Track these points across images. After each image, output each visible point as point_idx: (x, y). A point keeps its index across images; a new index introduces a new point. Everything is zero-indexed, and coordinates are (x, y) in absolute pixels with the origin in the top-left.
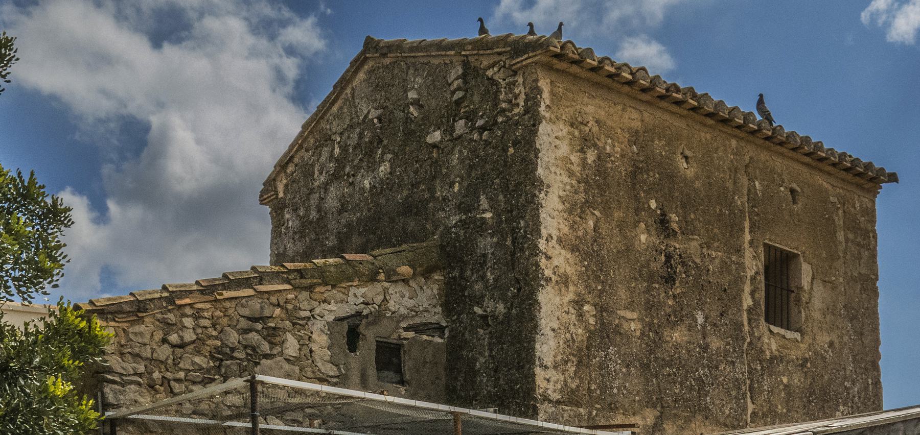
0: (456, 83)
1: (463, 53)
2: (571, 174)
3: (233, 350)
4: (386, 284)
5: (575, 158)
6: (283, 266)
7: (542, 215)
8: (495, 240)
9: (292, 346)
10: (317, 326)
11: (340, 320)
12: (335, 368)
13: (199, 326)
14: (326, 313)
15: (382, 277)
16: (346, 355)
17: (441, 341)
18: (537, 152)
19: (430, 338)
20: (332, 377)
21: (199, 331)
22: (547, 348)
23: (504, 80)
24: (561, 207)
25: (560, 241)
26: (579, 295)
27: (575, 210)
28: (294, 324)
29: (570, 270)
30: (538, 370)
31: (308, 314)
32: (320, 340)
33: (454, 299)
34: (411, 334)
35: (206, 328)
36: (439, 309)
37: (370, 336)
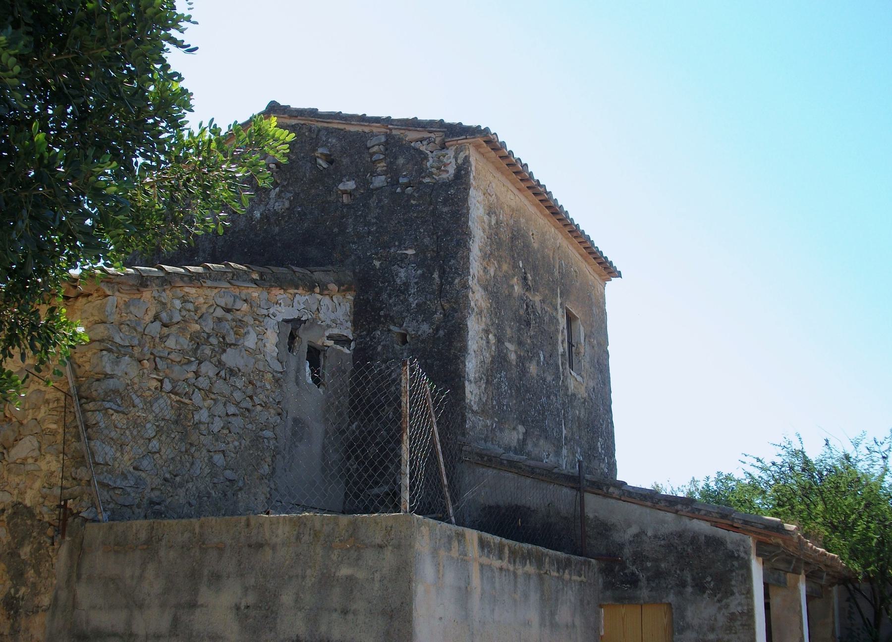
2: (484, 231)
4: (319, 297)
5: (486, 218)
7: (471, 258)
8: (419, 272)
10: (271, 322)
11: (287, 321)
12: (280, 365)
14: (278, 313)
15: (317, 290)
17: (348, 351)
19: (341, 348)
20: (276, 372)
21: (184, 313)
23: (432, 152)
25: (478, 281)
26: (487, 325)
27: (486, 257)
29: (483, 305)
30: (467, 383)
31: (265, 312)
32: (272, 338)
33: (366, 314)
34: (331, 343)
35: (189, 311)
36: (349, 324)
37: (306, 338)
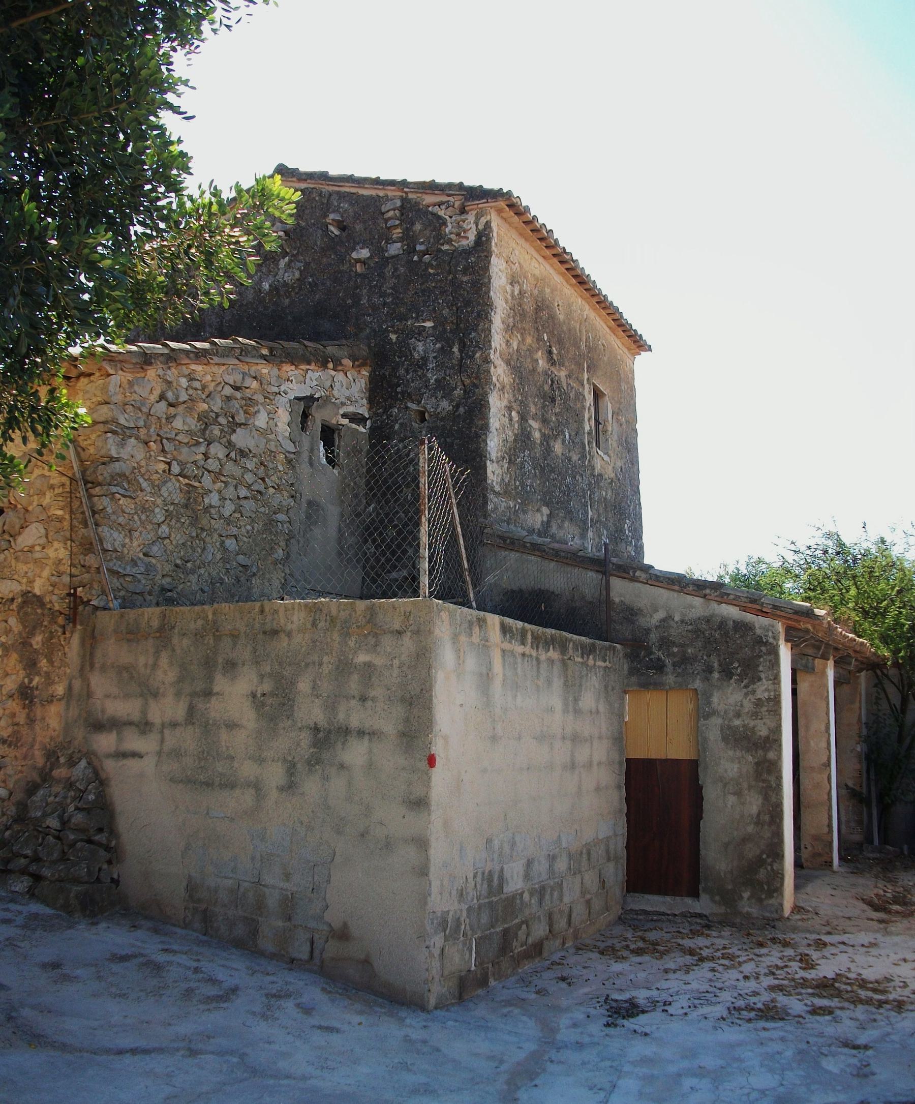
0: (391, 213)
1: (406, 190)
3: (217, 415)
5: (509, 288)
6: (167, 346)
7: (493, 331)
9: (261, 421)
10: (283, 401)
11: (298, 399)
13: (192, 388)
14: (289, 391)
15: (331, 365)
16: (300, 434)
18: (490, 278)
19: (357, 427)
22: (494, 445)
23: (451, 217)
24: (501, 326)
26: (510, 402)
27: (509, 329)
28: (265, 398)
30: (488, 463)
31: (276, 389)
32: (283, 417)
33: (382, 391)
34: (345, 421)
35: (196, 389)
36: (365, 401)
37: (319, 416)
